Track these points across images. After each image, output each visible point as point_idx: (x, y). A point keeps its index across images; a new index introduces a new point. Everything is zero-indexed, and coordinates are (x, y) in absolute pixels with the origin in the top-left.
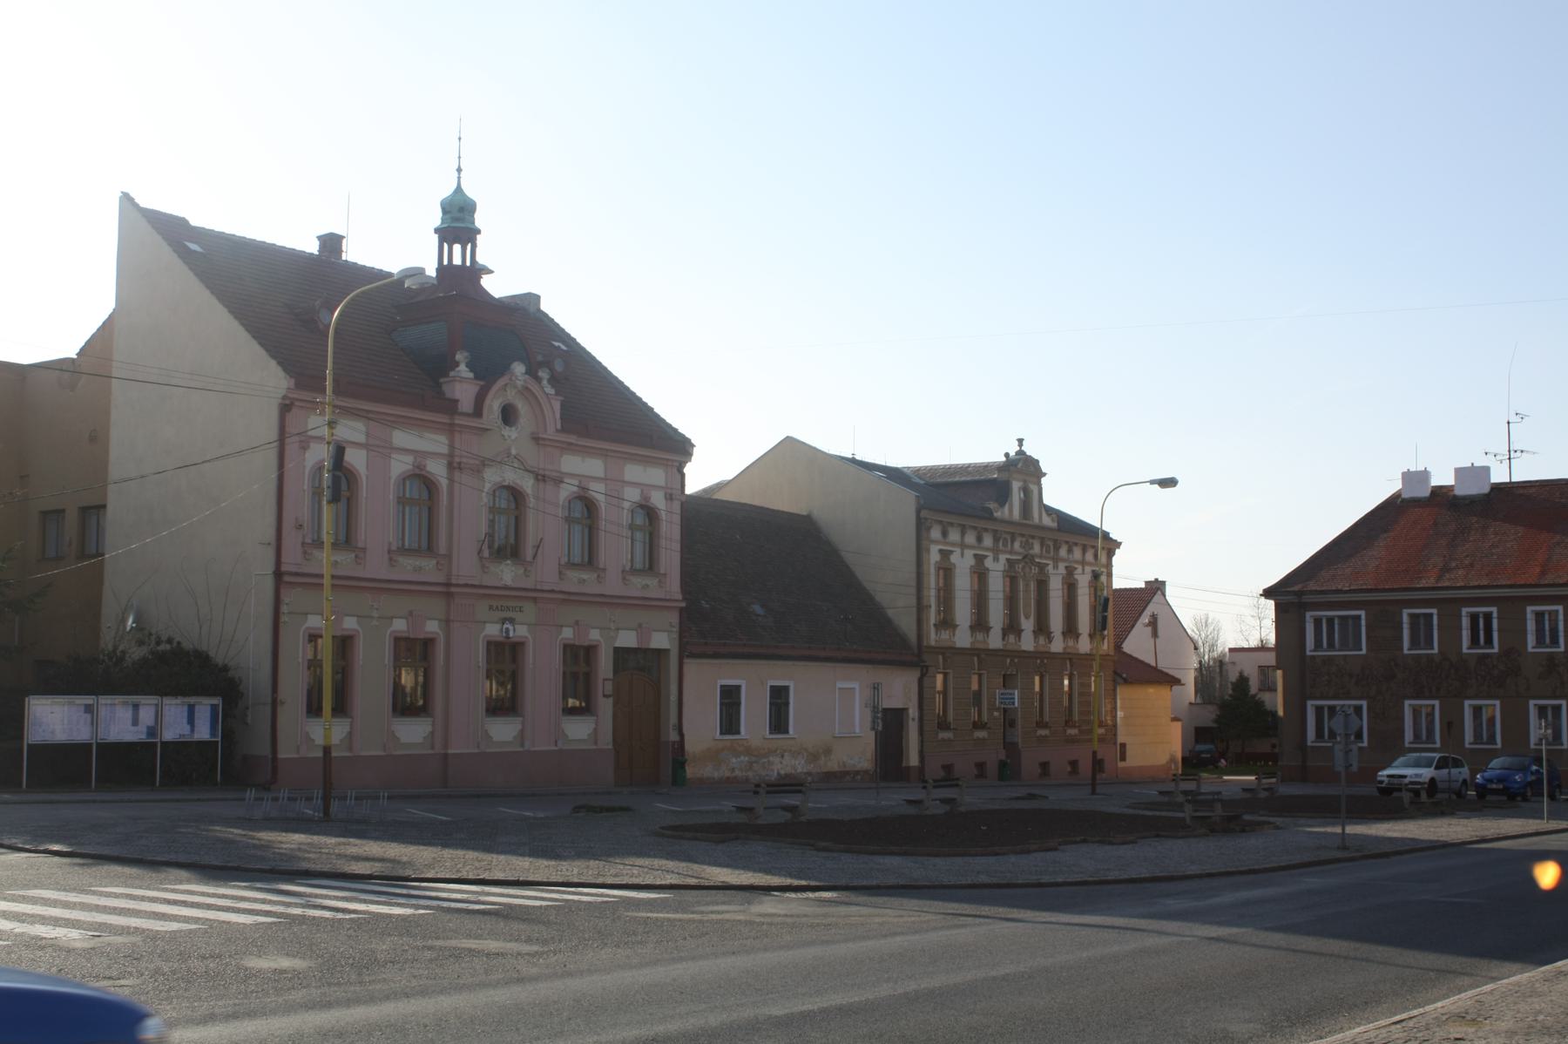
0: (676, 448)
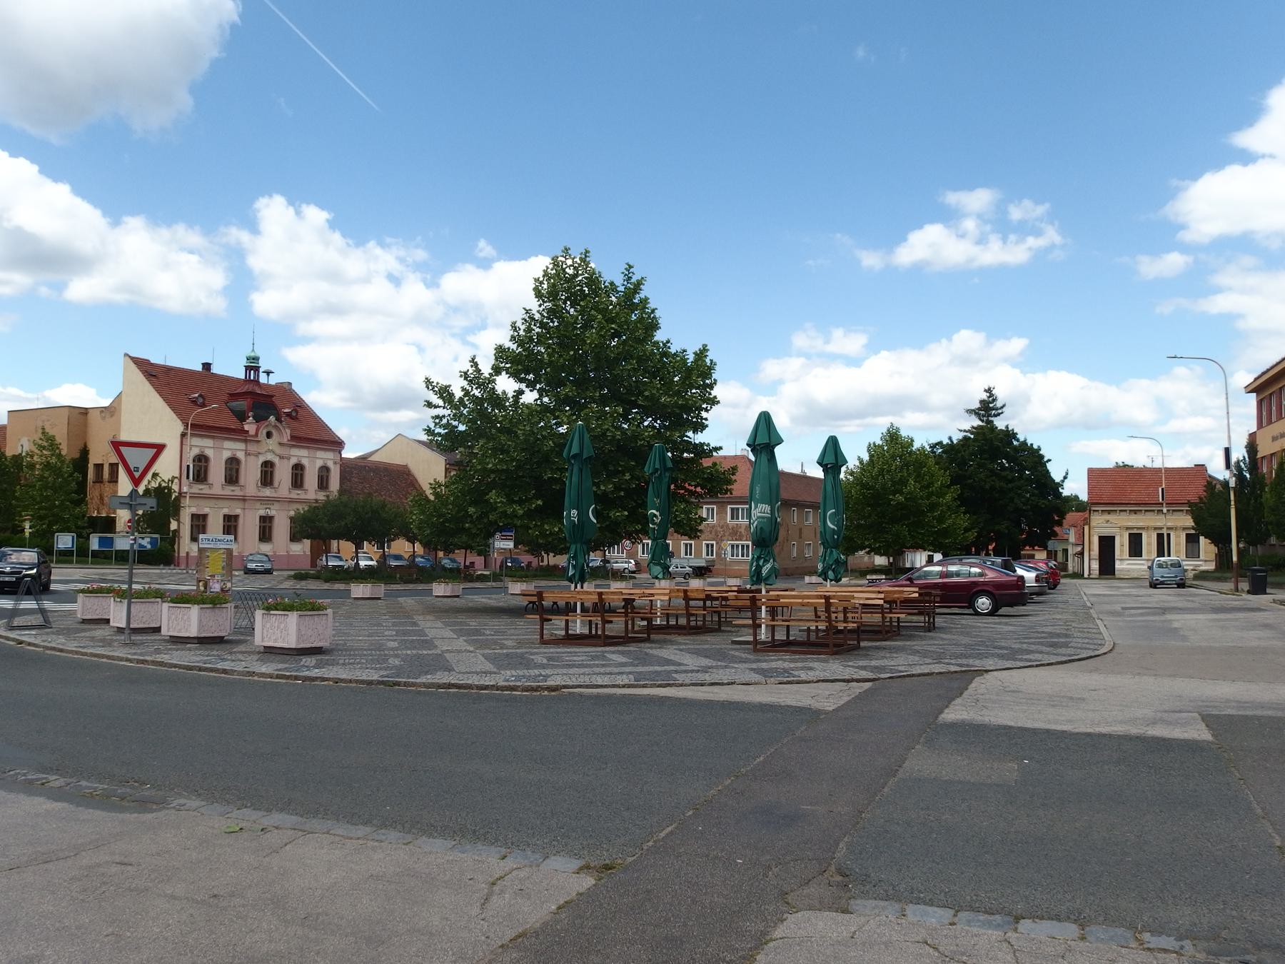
0: (337, 444)
